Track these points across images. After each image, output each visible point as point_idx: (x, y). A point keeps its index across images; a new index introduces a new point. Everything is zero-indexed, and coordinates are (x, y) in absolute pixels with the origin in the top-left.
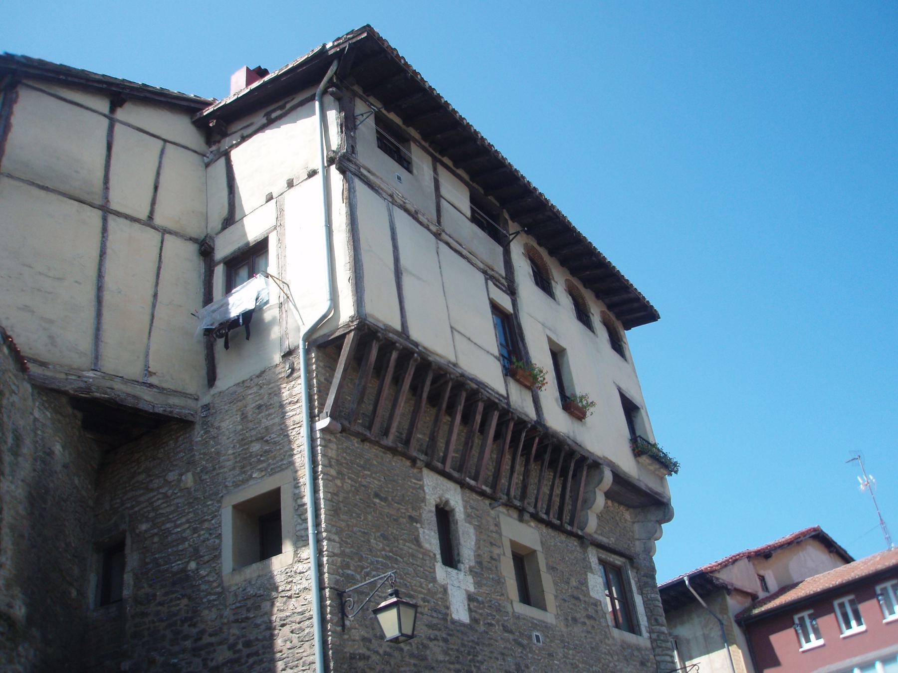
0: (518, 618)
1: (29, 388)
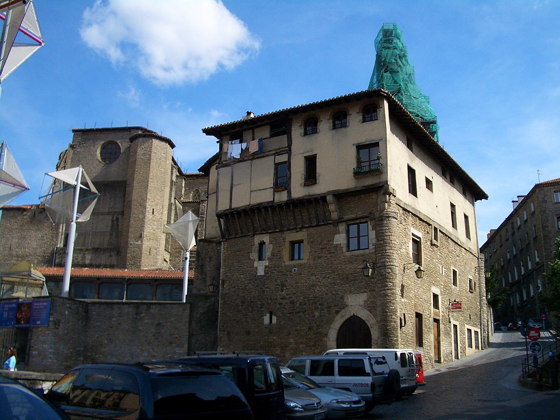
0: (287, 266)
1: (215, 244)
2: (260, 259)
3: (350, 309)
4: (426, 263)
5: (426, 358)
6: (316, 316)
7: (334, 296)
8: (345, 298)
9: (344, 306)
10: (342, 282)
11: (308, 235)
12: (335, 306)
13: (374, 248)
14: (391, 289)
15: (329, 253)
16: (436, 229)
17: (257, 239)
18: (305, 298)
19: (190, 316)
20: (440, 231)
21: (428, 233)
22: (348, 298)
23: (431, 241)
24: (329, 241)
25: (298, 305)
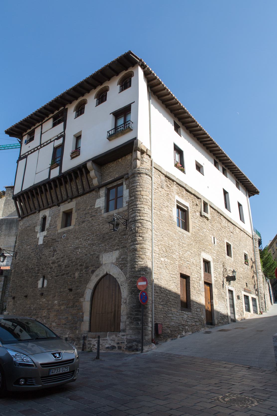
2: (43, 230)
3: (104, 267)
4: (194, 230)
5: (196, 320)
6: (76, 278)
7: (91, 257)
8: (101, 257)
9: (98, 265)
10: (99, 242)
11: (76, 204)
12: (92, 266)
13: (127, 205)
14: (140, 244)
15: (91, 217)
16: (205, 204)
17: (41, 214)
18: (69, 261)
19: (4, 286)
20: (211, 207)
21: (197, 205)
22: (102, 257)
23: (201, 213)
24: (91, 206)
25: (63, 267)
